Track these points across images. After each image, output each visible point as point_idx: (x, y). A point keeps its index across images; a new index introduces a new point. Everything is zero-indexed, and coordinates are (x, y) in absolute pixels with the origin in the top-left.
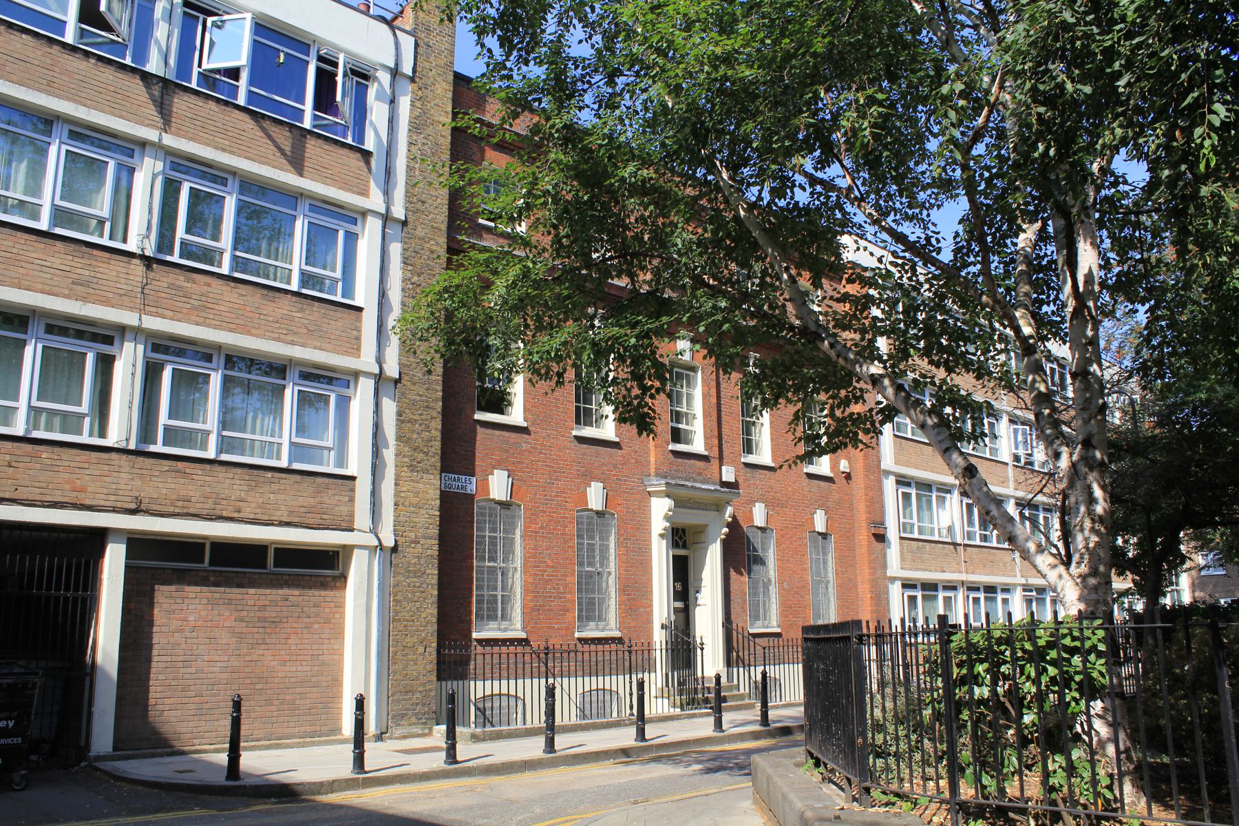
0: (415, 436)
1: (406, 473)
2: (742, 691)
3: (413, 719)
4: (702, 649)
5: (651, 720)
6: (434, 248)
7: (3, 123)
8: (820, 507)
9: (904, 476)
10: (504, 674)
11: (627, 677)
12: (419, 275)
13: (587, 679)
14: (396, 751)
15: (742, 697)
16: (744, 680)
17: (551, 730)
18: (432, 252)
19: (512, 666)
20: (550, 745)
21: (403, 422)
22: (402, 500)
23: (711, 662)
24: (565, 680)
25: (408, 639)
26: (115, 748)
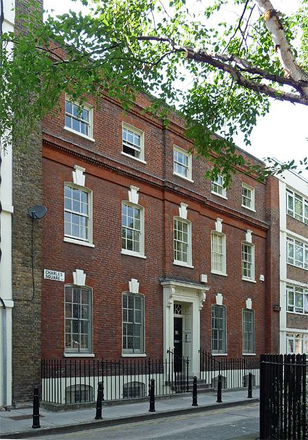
0: (25, 247)
1: (19, 267)
2: (207, 383)
3: (27, 399)
4: (188, 363)
5: (159, 398)
6: (34, 138)
7: (20, 8)
8: (249, 297)
9: (291, 284)
10: (78, 372)
11: (148, 375)
12: (24, 153)
13: (125, 377)
14: (11, 418)
15: (207, 386)
16: (210, 376)
17: (152, 398)
18: (32, 140)
19: (140, 364)
20: (152, 408)
21: (17, 238)
22: (18, 283)
23: (194, 369)
24: (121, 377)
25: (24, 357)
26: (125, 395)
